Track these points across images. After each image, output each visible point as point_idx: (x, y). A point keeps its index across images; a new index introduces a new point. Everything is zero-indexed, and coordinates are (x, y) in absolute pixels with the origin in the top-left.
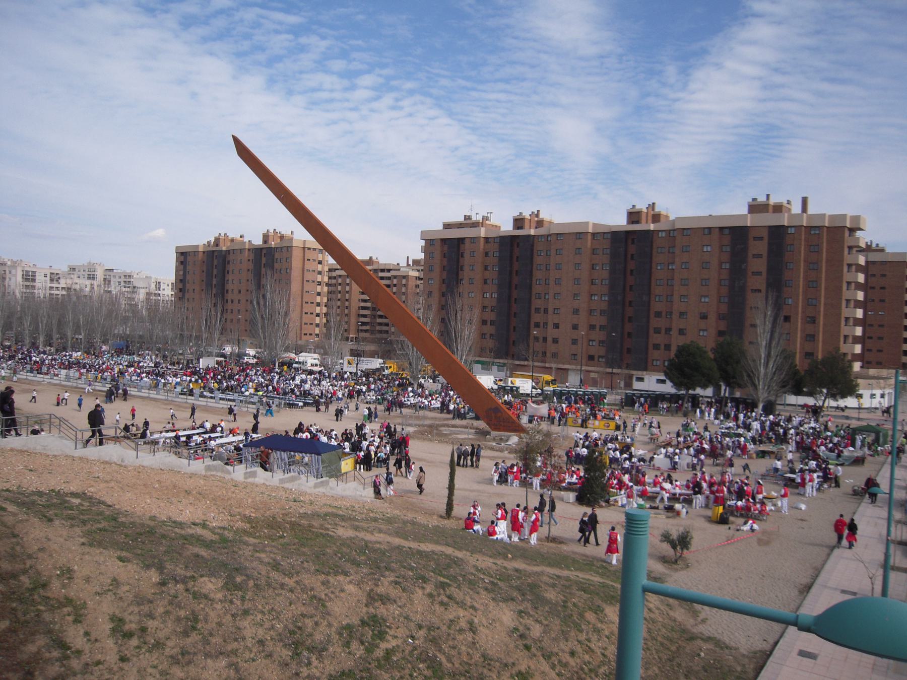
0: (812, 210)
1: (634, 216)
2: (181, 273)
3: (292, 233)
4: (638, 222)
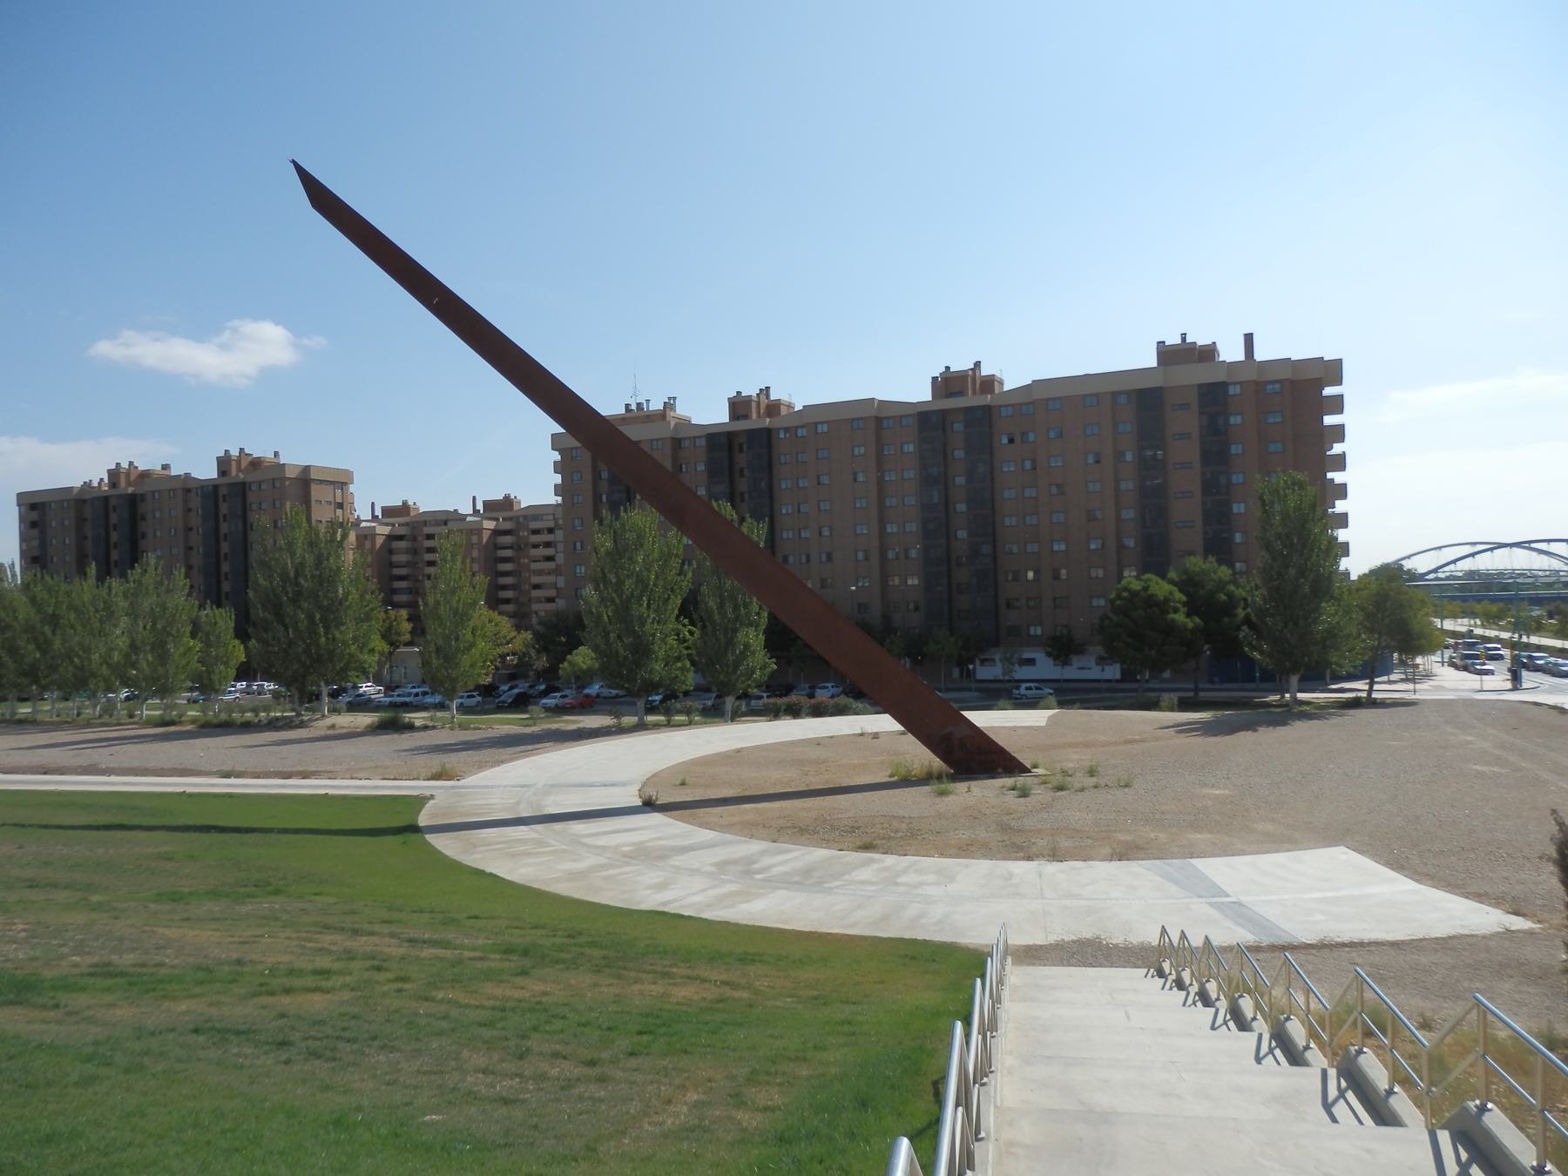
0: (1259, 356)
1: (739, 406)
2: (35, 543)
3: (276, 454)
4: (746, 417)
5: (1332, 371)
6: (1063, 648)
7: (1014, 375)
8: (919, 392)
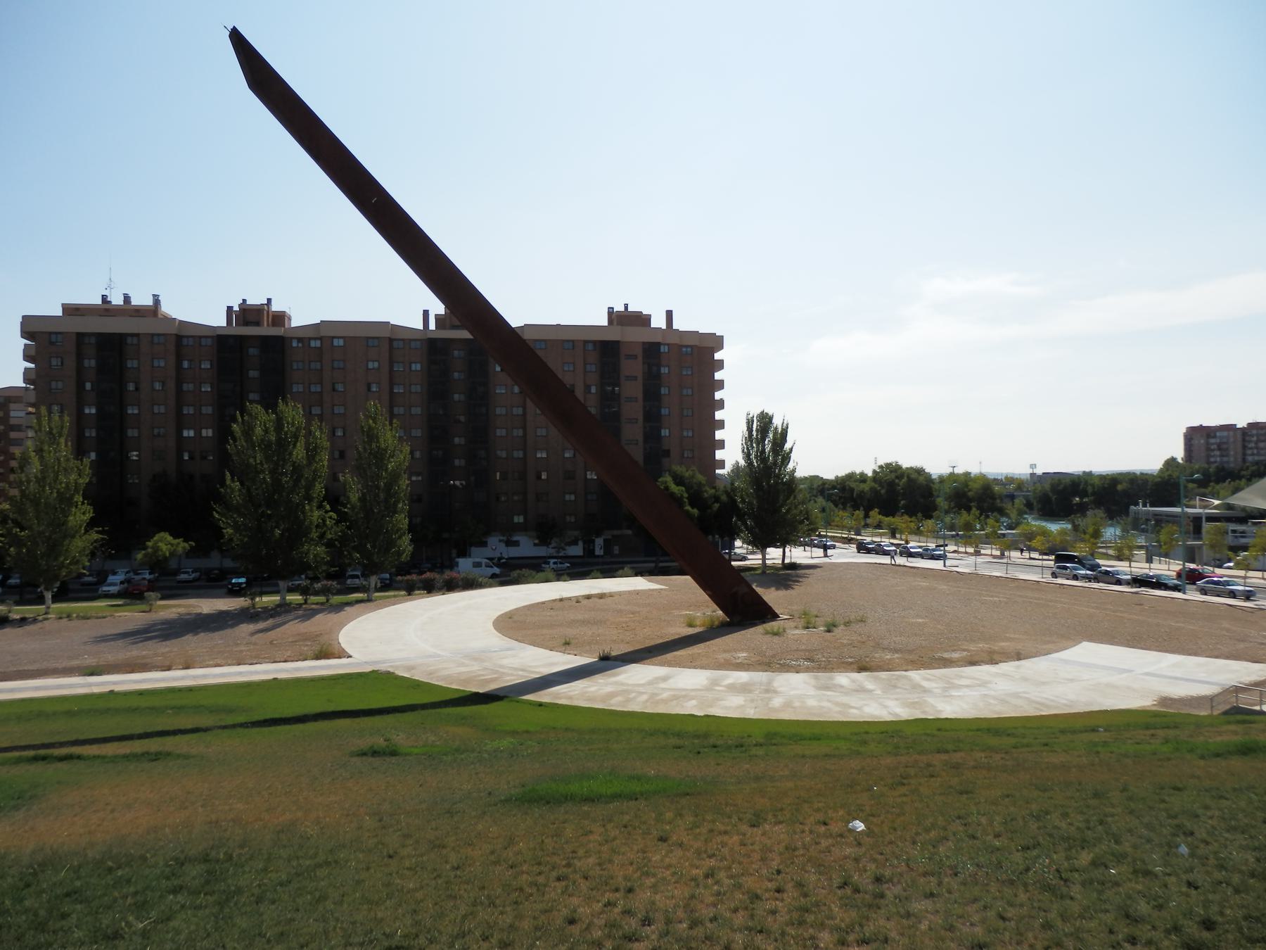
5: (716, 342)
6: (545, 531)
7: (302, 315)
8: (217, 319)
